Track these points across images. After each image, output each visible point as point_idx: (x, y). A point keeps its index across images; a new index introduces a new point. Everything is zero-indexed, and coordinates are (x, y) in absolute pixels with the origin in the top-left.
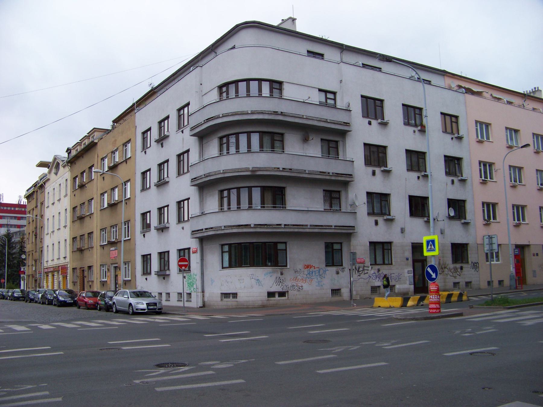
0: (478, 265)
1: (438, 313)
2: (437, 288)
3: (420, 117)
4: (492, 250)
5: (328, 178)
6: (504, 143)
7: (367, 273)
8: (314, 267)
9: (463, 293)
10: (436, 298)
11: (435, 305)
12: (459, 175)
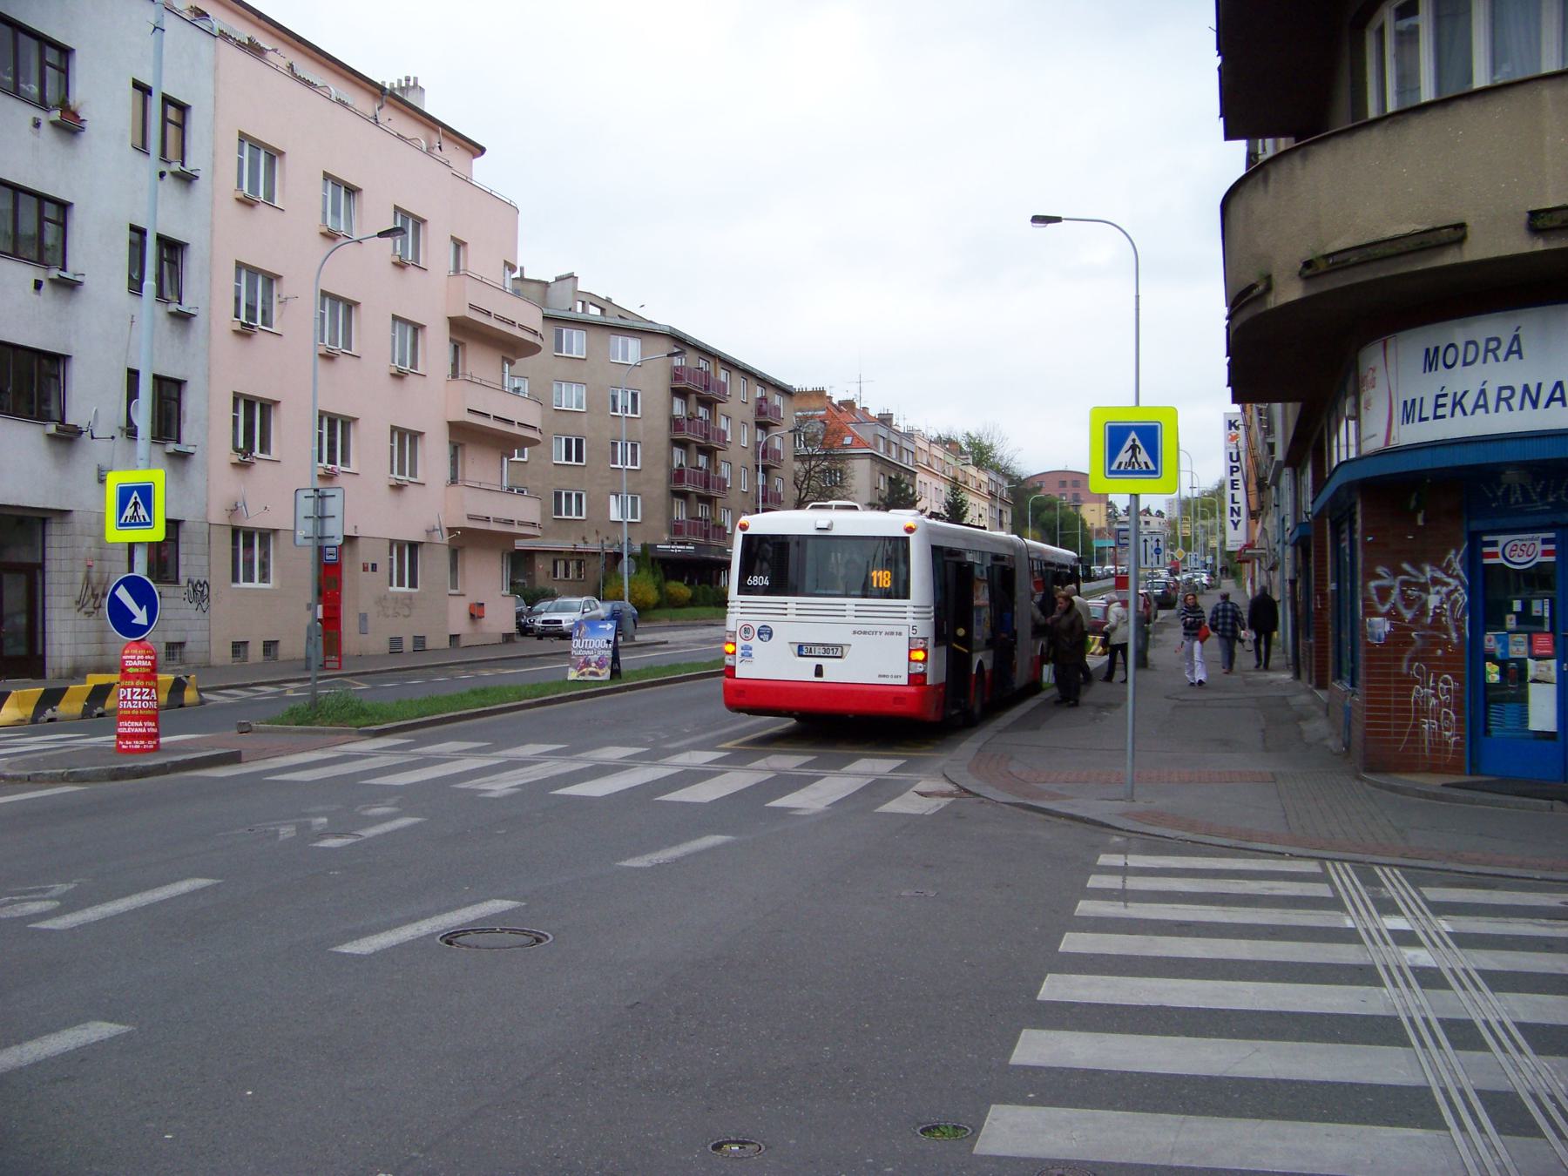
0: (206, 590)
1: (151, 754)
2: (149, 664)
3: (60, 78)
4: (321, 538)
6: (314, 224)
9: (184, 679)
10: (144, 698)
11: (141, 724)
12: (170, 298)
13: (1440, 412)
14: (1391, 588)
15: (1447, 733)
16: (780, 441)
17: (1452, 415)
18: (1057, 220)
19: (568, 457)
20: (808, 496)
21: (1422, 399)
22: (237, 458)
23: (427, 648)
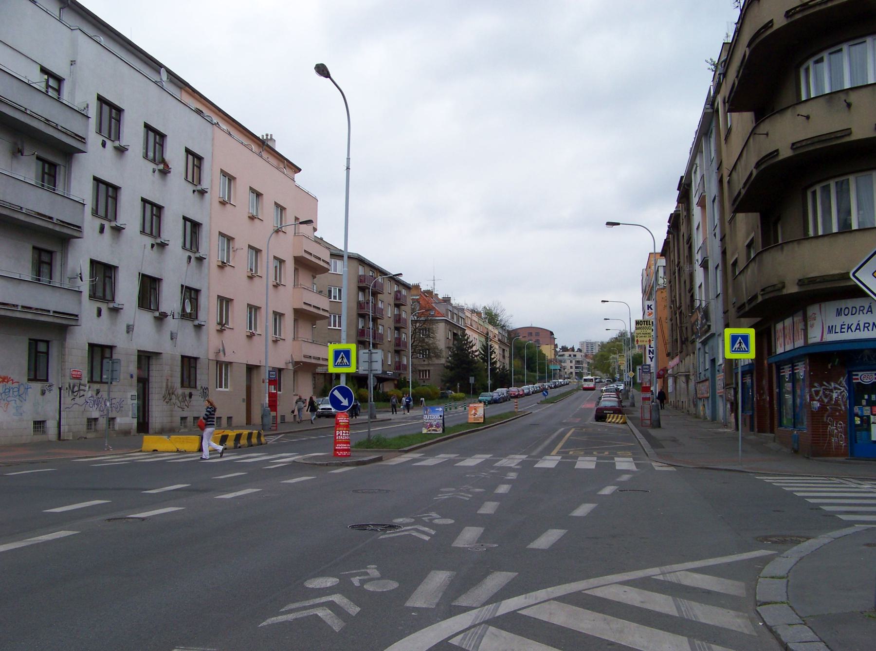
5: (51, 226)
7: (83, 395)
8: (11, 381)
13: (843, 330)
14: (820, 391)
15: (841, 442)
16: (406, 315)
17: (847, 332)
18: (618, 224)
19: (335, 326)
20: (415, 343)
21: (836, 326)
22: (219, 327)
23: (286, 421)
